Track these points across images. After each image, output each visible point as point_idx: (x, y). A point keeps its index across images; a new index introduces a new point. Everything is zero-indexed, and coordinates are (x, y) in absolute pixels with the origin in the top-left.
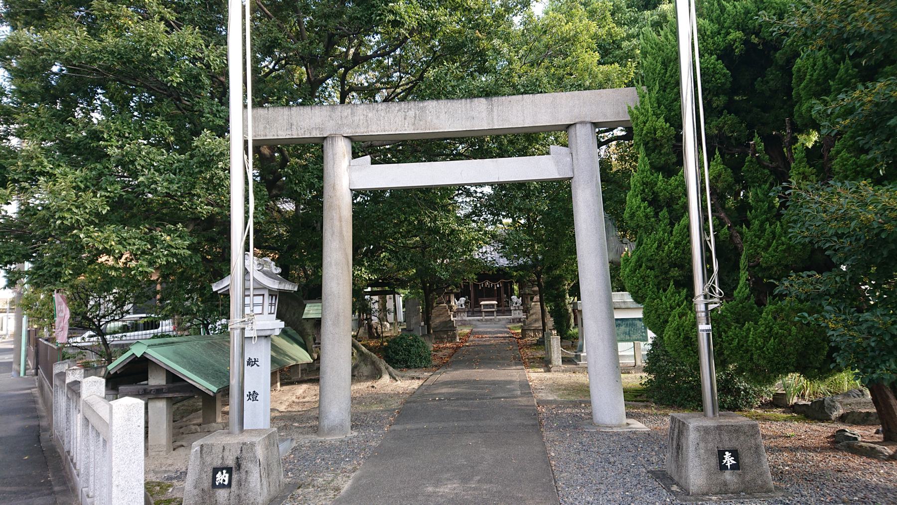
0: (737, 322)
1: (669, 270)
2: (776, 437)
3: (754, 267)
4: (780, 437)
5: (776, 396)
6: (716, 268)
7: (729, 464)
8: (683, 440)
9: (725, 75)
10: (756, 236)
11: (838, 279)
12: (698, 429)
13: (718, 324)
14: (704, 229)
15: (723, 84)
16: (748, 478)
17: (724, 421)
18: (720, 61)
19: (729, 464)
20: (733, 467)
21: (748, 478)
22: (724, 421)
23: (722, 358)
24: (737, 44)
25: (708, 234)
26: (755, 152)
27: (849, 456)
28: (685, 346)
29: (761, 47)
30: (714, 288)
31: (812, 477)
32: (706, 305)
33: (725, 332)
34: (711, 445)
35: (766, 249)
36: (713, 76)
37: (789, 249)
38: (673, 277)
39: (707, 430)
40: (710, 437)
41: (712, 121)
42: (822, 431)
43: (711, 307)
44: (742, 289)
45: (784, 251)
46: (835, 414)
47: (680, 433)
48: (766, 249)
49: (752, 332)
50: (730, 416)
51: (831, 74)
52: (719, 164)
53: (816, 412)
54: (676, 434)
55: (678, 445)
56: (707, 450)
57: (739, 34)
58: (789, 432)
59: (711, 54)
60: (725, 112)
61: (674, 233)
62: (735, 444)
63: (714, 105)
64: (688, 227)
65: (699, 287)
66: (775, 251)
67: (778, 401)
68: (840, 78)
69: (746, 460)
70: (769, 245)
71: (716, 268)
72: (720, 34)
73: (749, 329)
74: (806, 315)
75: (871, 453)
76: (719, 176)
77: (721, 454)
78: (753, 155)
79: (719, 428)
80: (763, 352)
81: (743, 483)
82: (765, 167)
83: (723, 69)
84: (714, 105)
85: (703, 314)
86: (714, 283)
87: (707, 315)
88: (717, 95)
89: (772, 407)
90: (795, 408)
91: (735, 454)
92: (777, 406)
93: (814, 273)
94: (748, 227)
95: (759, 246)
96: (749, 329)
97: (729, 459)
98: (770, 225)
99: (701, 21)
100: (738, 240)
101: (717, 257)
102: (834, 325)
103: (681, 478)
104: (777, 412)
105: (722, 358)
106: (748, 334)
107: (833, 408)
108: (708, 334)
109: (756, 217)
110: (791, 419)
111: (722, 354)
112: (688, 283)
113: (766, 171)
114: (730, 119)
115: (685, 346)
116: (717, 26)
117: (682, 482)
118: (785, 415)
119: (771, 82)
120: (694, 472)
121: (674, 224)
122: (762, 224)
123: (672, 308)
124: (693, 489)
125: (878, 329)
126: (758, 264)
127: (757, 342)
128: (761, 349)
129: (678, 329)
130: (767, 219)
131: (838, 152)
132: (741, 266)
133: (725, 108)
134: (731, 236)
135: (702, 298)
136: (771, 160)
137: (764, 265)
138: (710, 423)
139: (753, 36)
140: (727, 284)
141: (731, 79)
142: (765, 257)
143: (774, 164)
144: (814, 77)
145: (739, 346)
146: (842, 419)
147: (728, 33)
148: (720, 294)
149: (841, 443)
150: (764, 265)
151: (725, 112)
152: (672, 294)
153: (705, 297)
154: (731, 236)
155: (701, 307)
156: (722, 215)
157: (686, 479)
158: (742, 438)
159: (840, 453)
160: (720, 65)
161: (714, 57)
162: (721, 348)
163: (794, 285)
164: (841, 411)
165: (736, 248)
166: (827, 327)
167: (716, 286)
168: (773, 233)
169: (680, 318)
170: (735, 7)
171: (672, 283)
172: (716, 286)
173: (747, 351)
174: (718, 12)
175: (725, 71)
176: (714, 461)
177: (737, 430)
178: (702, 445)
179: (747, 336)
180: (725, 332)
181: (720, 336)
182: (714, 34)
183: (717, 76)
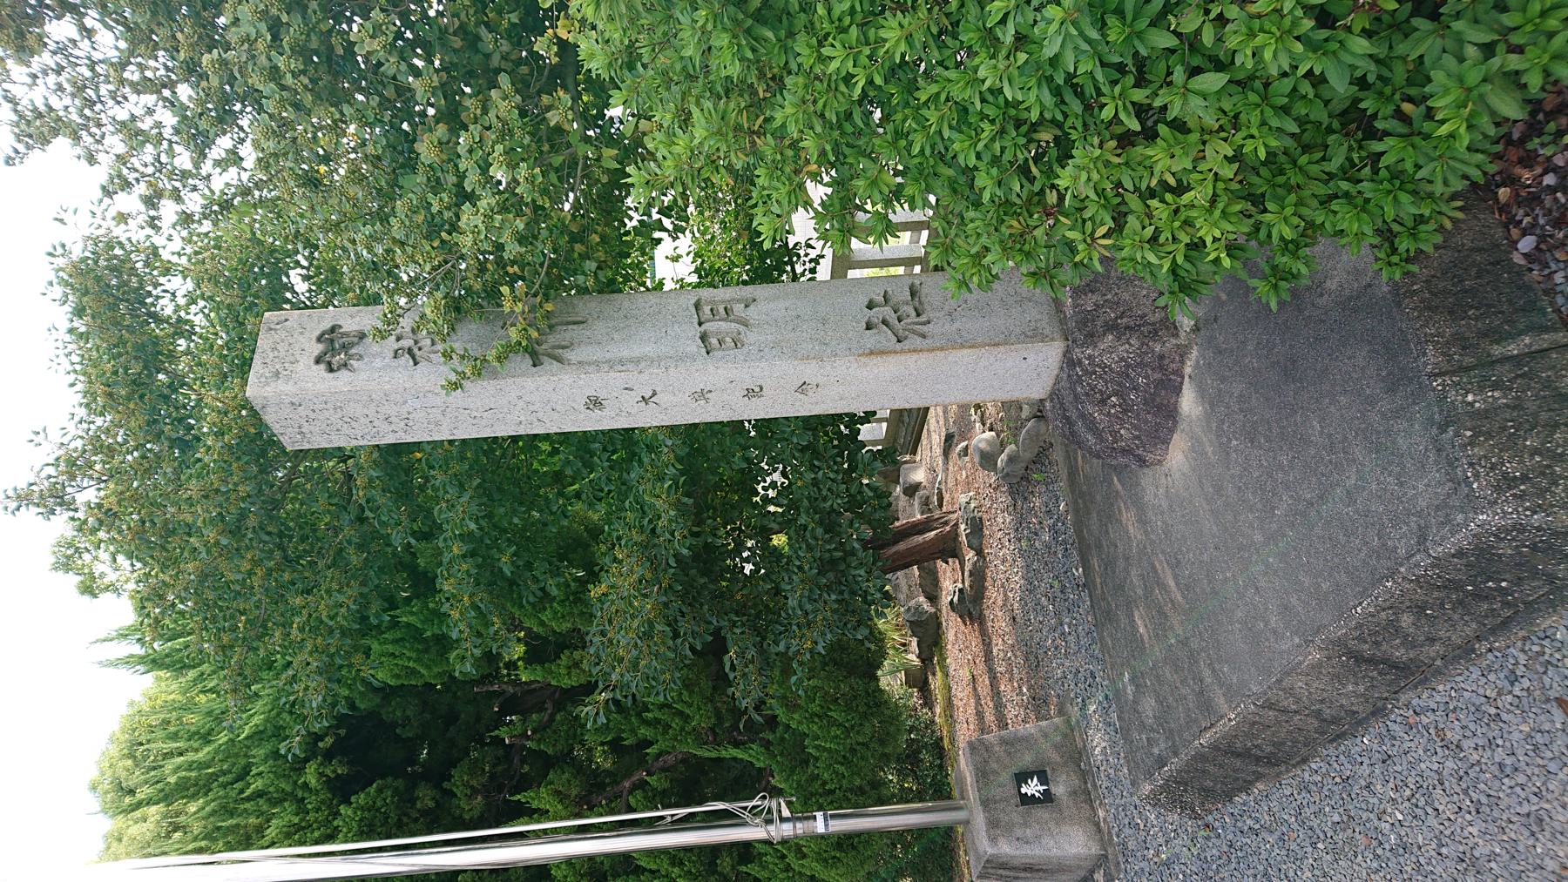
0: (807, 762)
1: (721, 874)
2: (978, 698)
3: (715, 734)
4: (975, 689)
5: (910, 682)
6: (720, 806)
7: (1041, 788)
8: (1016, 862)
9: (380, 791)
10: (665, 732)
11: (738, 631)
12: (993, 840)
13: (812, 794)
14: (650, 826)
15: (396, 791)
16: (1055, 757)
17: (972, 794)
18: (353, 799)
19: (1041, 788)
20: (1043, 780)
21: (1055, 757)
22: (972, 794)
23: (867, 788)
24: (328, 772)
25: (662, 818)
26: (524, 735)
27: (987, 602)
28: (854, 848)
29: (342, 732)
30: (754, 807)
31: (1032, 658)
32: (782, 820)
33: (824, 783)
34: (1016, 818)
35: (687, 719)
36: (378, 810)
37: (688, 685)
38: (733, 867)
39: (993, 824)
40: (1004, 818)
41: (458, 806)
42: (954, 629)
43: (786, 813)
44: (753, 755)
45: (691, 693)
46: (927, 606)
47: (1004, 866)
48: (687, 719)
49: (822, 742)
50: (961, 781)
51: (415, 634)
52: (537, 793)
53: (929, 634)
54: (1008, 873)
55: (1025, 870)
56: (1025, 825)
57: (311, 768)
58: (965, 674)
59: (337, 814)
60: (446, 785)
61: (654, 867)
62: (1006, 777)
63: (431, 804)
64: (652, 853)
65: (752, 833)
66: (690, 705)
67: (918, 681)
68: (423, 622)
69: (1027, 760)
70: (681, 713)
71: (720, 806)
72: (303, 799)
73: (817, 747)
74: (794, 679)
75: (979, 576)
76: (558, 793)
77: (1026, 800)
78: (528, 738)
79: (985, 803)
80: (853, 727)
81: (1065, 764)
82: (552, 719)
83: (368, 794)
84: (431, 804)
85: (799, 825)
86: (745, 808)
87: (799, 819)
88: (413, 801)
89: (930, 691)
90: (926, 658)
91: (1022, 777)
92: (926, 682)
93: (726, 658)
94: (650, 744)
95: (682, 729)
96: (817, 747)
97: (1033, 788)
98: (648, 711)
99: (271, 832)
100: (671, 759)
101: (700, 804)
102: (811, 642)
103: (1079, 867)
104: (936, 682)
105: (867, 788)
106: (825, 749)
107: (918, 607)
108: (833, 816)
109: (633, 731)
110: (943, 659)
111: (860, 788)
112: (745, 850)
113: (558, 717)
114: (460, 779)
115: (854, 848)
116: (286, 804)
117: (1088, 864)
118: (939, 674)
119: (408, 713)
120: (1067, 847)
121: (639, 867)
122: (647, 723)
123: (788, 868)
124: (1095, 849)
125: (811, 590)
126: (712, 729)
127: (837, 737)
128: (847, 731)
129: (825, 861)
130: (639, 715)
131: (542, 623)
132: (714, 755)
133: (438, 786)
134: (663, 770)
135: (771, 828)
136: (541, 709)
137: (713, 720)
138: (980, 819)
139: (321, 744)
140: (744, 783)
141: (389, 779)
142: (701, 720)
143: (549, 705)
144: (414, 655)
145: (845, 761)
146: (933, 598)
147: (306, 785)
148: (764, 797)
149: (971, 606)
150: (713, 720)
151: (446, 785)
152: (764, 868)
153: (769, 822)
154: (663, 770)
155: (787, 830)
156: (627, 784)
157: (1080, 859)
158: (995, 766)
159: (986, 612)
160: (360, 799)
161: (343, 809)
162: (851, 790)
163: (745, 691)
164: (922, 599)
165: (684, 761)
166: (811, 651)
167: (750, 804)
168: (662, 706)
169: (804, 856)
170: (260, 774)
171: (744, 869)
172: (750, 804)
173: (853, 751)
174: (261, 802)
175: (372, 789)
176: (1041, 813)
177: (983, 775)
178: (1019, 832)
179: (829, 750)
180: (824, 783)
181: (832, 792)
182: (301, 809)
183: (379, 804)
